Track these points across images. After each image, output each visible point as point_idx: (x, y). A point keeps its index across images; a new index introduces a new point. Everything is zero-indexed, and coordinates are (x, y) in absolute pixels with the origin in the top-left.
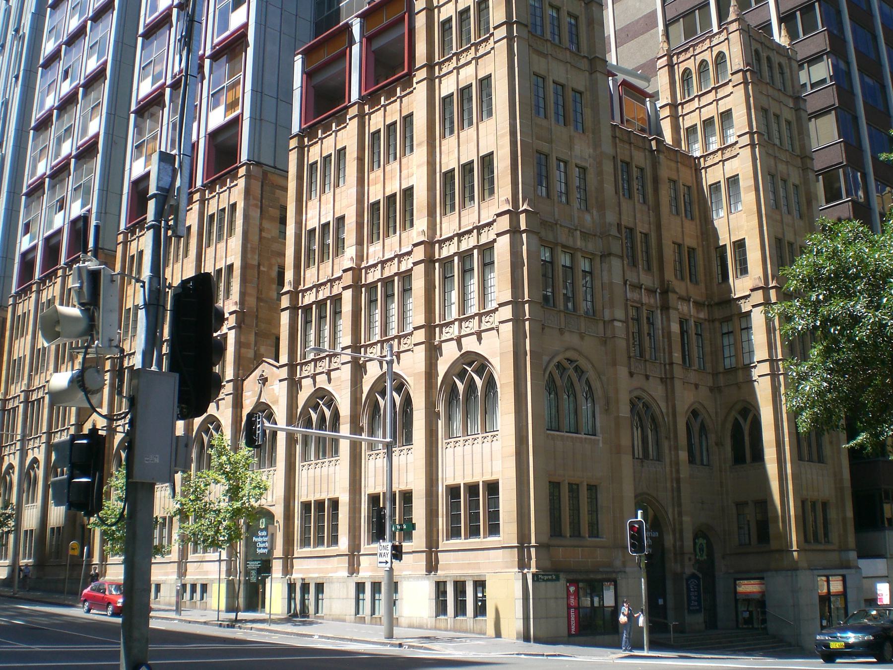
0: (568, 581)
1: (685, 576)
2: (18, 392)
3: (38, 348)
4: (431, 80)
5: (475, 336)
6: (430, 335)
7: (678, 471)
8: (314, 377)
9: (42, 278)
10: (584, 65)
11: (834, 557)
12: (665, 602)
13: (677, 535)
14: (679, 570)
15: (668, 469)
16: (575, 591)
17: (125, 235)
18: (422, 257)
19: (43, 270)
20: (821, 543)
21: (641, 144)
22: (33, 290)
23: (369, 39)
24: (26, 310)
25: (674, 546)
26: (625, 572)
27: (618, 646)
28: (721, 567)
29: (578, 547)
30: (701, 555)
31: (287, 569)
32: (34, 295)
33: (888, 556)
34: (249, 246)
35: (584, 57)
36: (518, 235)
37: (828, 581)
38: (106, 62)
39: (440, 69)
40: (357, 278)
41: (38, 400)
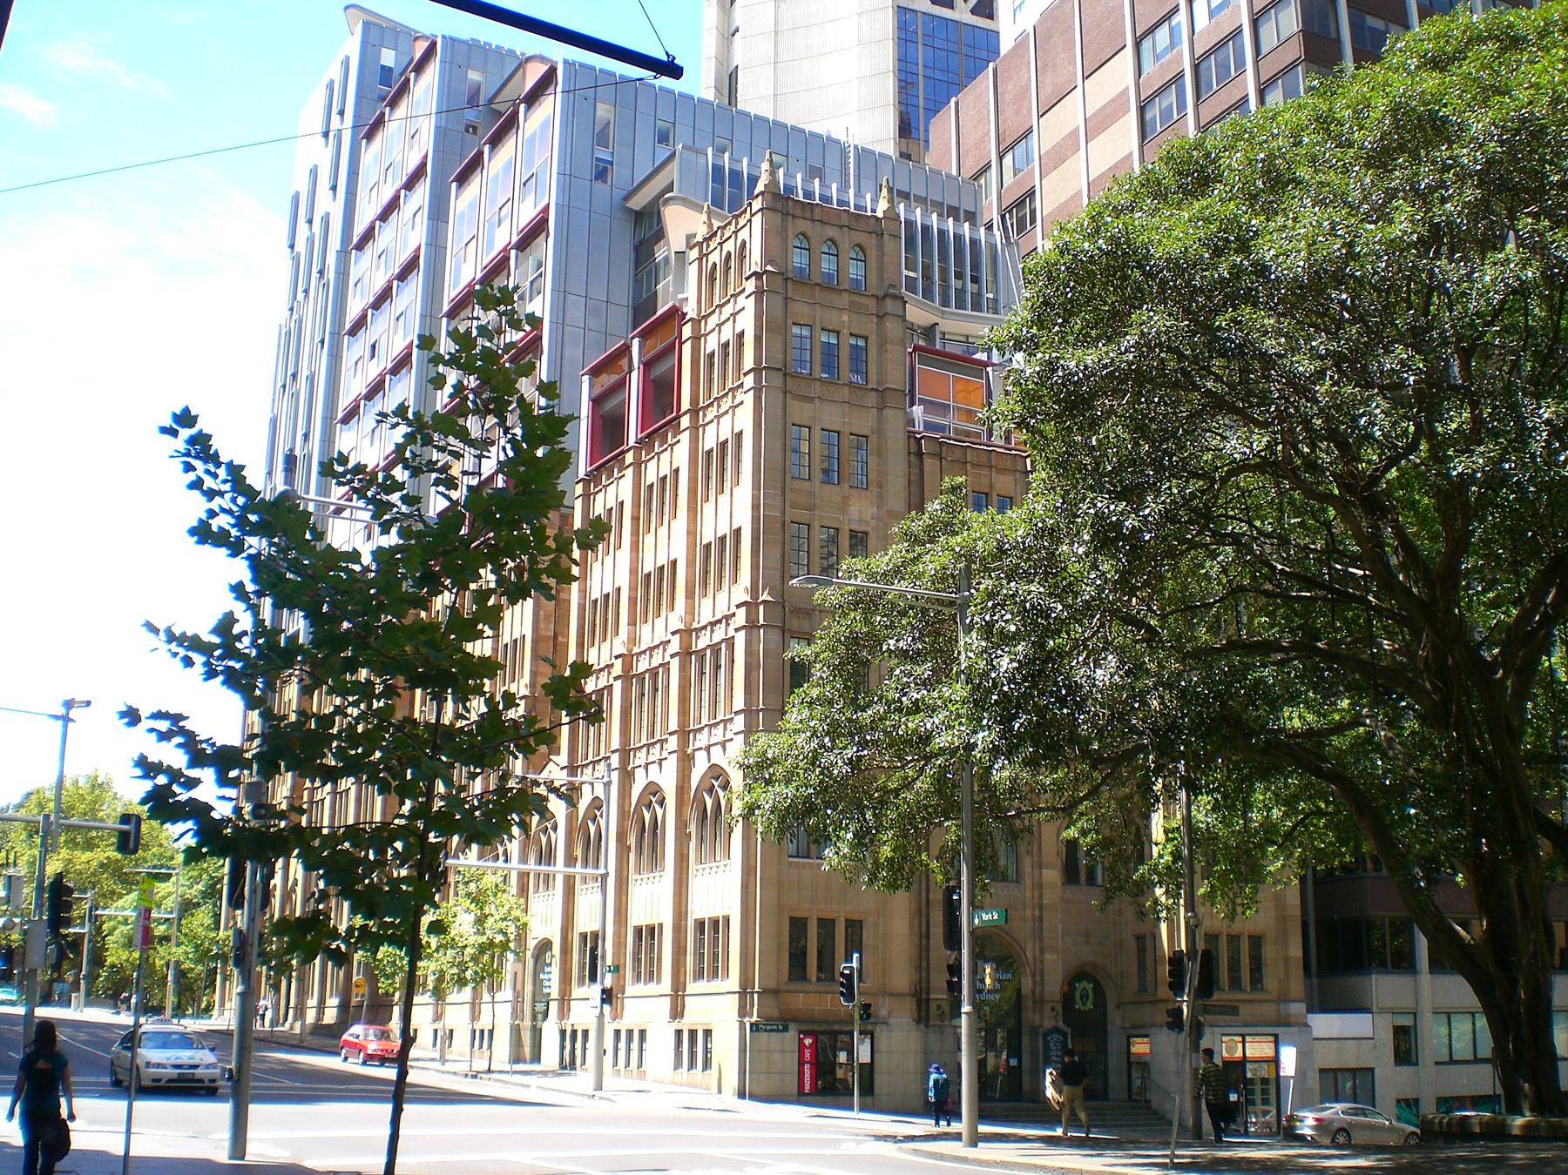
0: (800, 1032)
1: (1041, 1030)
2: (660, 636)
3: (645, 571)
4: (695, 428)
5: (719, 746)
6: (625, 760)
7: (1041, 897)
8: (708, 749)
9: (591, 472)
10: (872, 399)
11: (1268, 1010)
12: (1020, 1062)
13: (1038, 978)
14: (1037, 1021)
15: (1028, 894)
16: (811, 1045)
17: (637, 450)
18: (743, 623)
19: (644, 423)
20: (1245, 991)
21: (1009, 465)
22: (627, 463)
23: (648, 365)
24: (611, 503)
25: (1033, 992)
26: (887, 1024)
27: (851, 1108)
28: (1115, 1019)
29: (827, 993)
30: (1084, 1004)
31: (564, 1012)
32: (685, 437)
33: (1375, 1009)
34: (542, 613)
35: (872, 389)
36: (755, 631)
37: (1244, 1042)
38: (546, 209)
39: (705, 415)
40: (627, 667)
41: (653, 673)
